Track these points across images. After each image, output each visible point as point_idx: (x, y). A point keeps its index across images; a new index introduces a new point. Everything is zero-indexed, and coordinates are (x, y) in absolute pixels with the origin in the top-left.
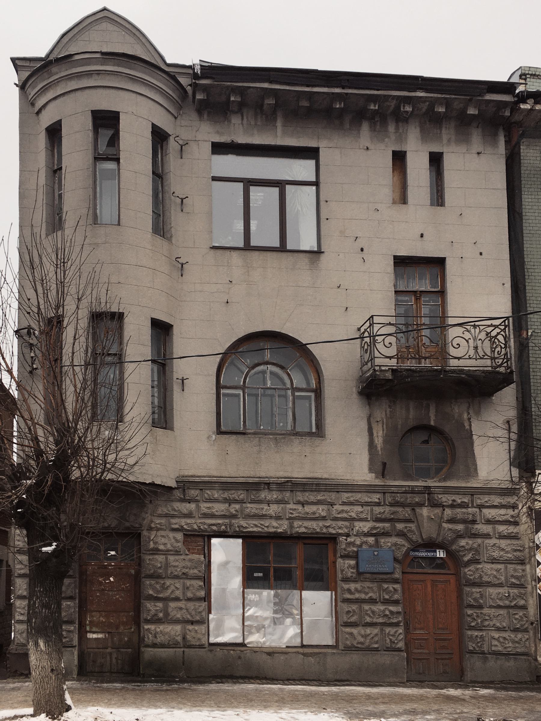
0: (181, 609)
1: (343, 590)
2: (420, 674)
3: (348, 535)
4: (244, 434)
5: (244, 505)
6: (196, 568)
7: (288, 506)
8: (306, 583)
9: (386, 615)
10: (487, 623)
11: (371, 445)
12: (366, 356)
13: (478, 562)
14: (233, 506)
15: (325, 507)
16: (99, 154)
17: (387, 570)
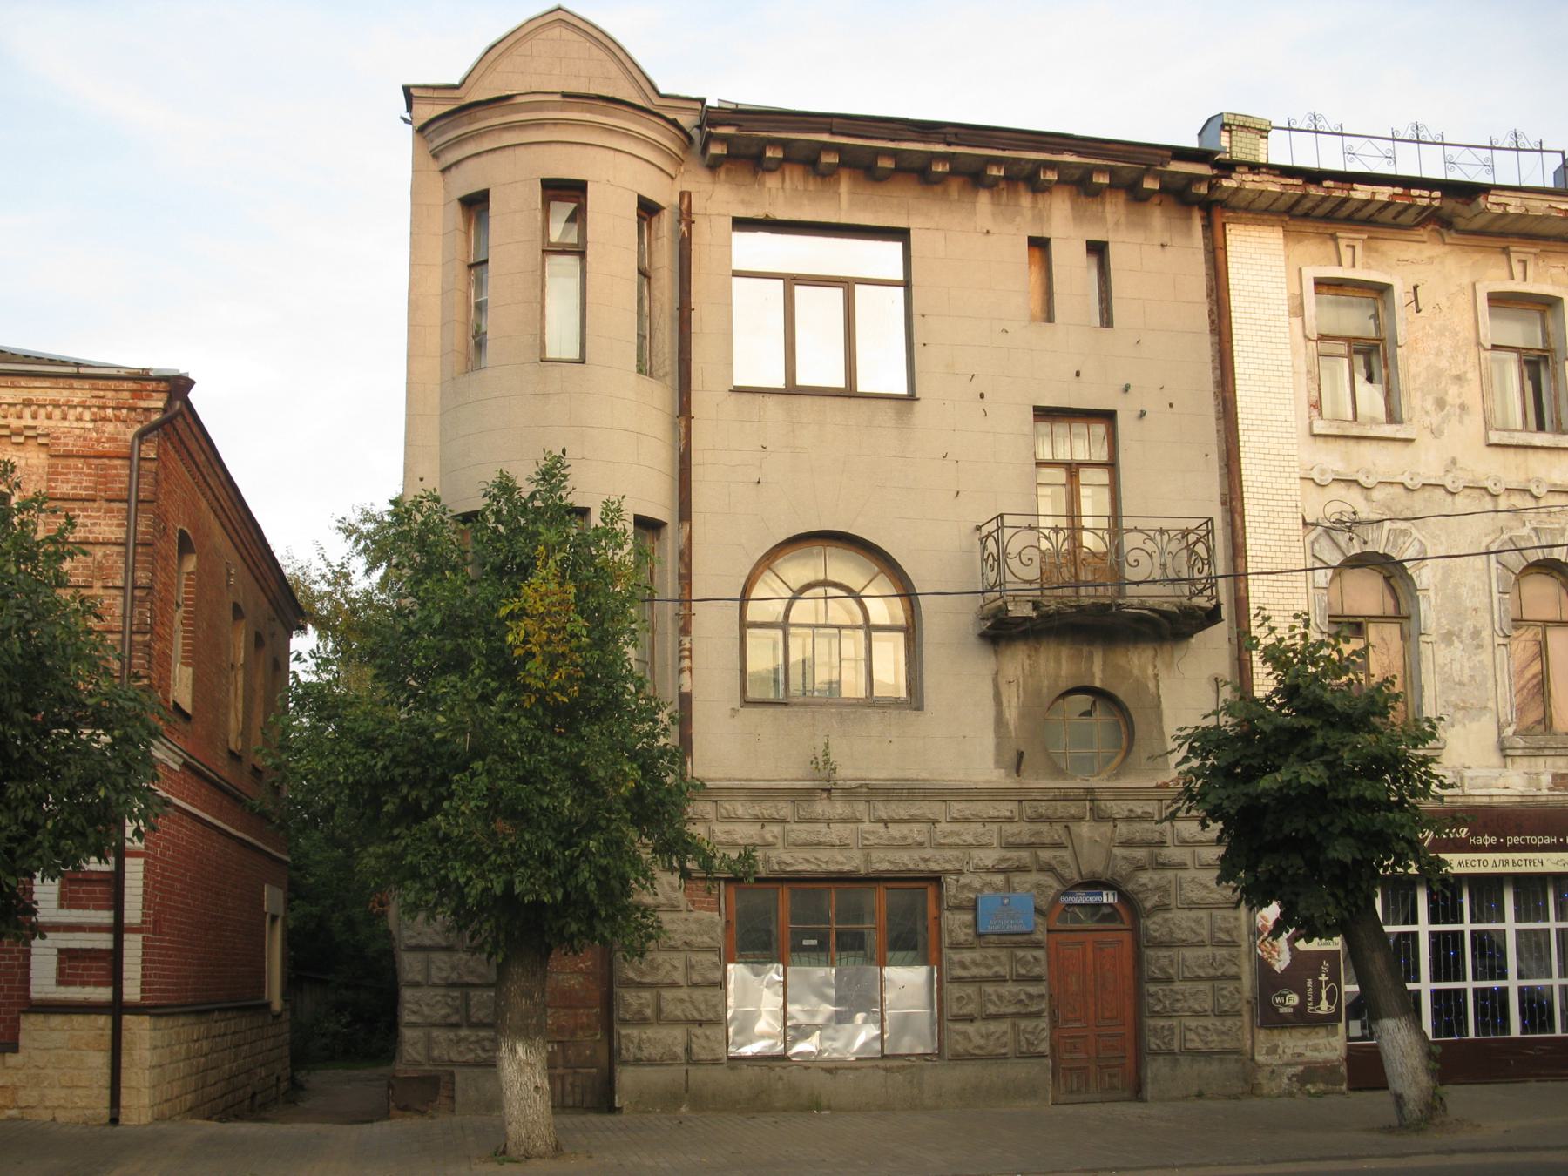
0: (682, 1001)
1: (951, 963)
2: (1072, 1092)
3: (960, 872)
4: (786, 704)
5: (788, 826)
6: (707, 933)
7: (861, 826)
8: (889, 955)
9: (1021, 1001)
10: (1179, 1005)
11: (1000, 722)
12: (992, 577)
13: (1165, 908)
14: (768, 827)
15: (925, 827)
16: (550, 244)
17: (1024, 928)
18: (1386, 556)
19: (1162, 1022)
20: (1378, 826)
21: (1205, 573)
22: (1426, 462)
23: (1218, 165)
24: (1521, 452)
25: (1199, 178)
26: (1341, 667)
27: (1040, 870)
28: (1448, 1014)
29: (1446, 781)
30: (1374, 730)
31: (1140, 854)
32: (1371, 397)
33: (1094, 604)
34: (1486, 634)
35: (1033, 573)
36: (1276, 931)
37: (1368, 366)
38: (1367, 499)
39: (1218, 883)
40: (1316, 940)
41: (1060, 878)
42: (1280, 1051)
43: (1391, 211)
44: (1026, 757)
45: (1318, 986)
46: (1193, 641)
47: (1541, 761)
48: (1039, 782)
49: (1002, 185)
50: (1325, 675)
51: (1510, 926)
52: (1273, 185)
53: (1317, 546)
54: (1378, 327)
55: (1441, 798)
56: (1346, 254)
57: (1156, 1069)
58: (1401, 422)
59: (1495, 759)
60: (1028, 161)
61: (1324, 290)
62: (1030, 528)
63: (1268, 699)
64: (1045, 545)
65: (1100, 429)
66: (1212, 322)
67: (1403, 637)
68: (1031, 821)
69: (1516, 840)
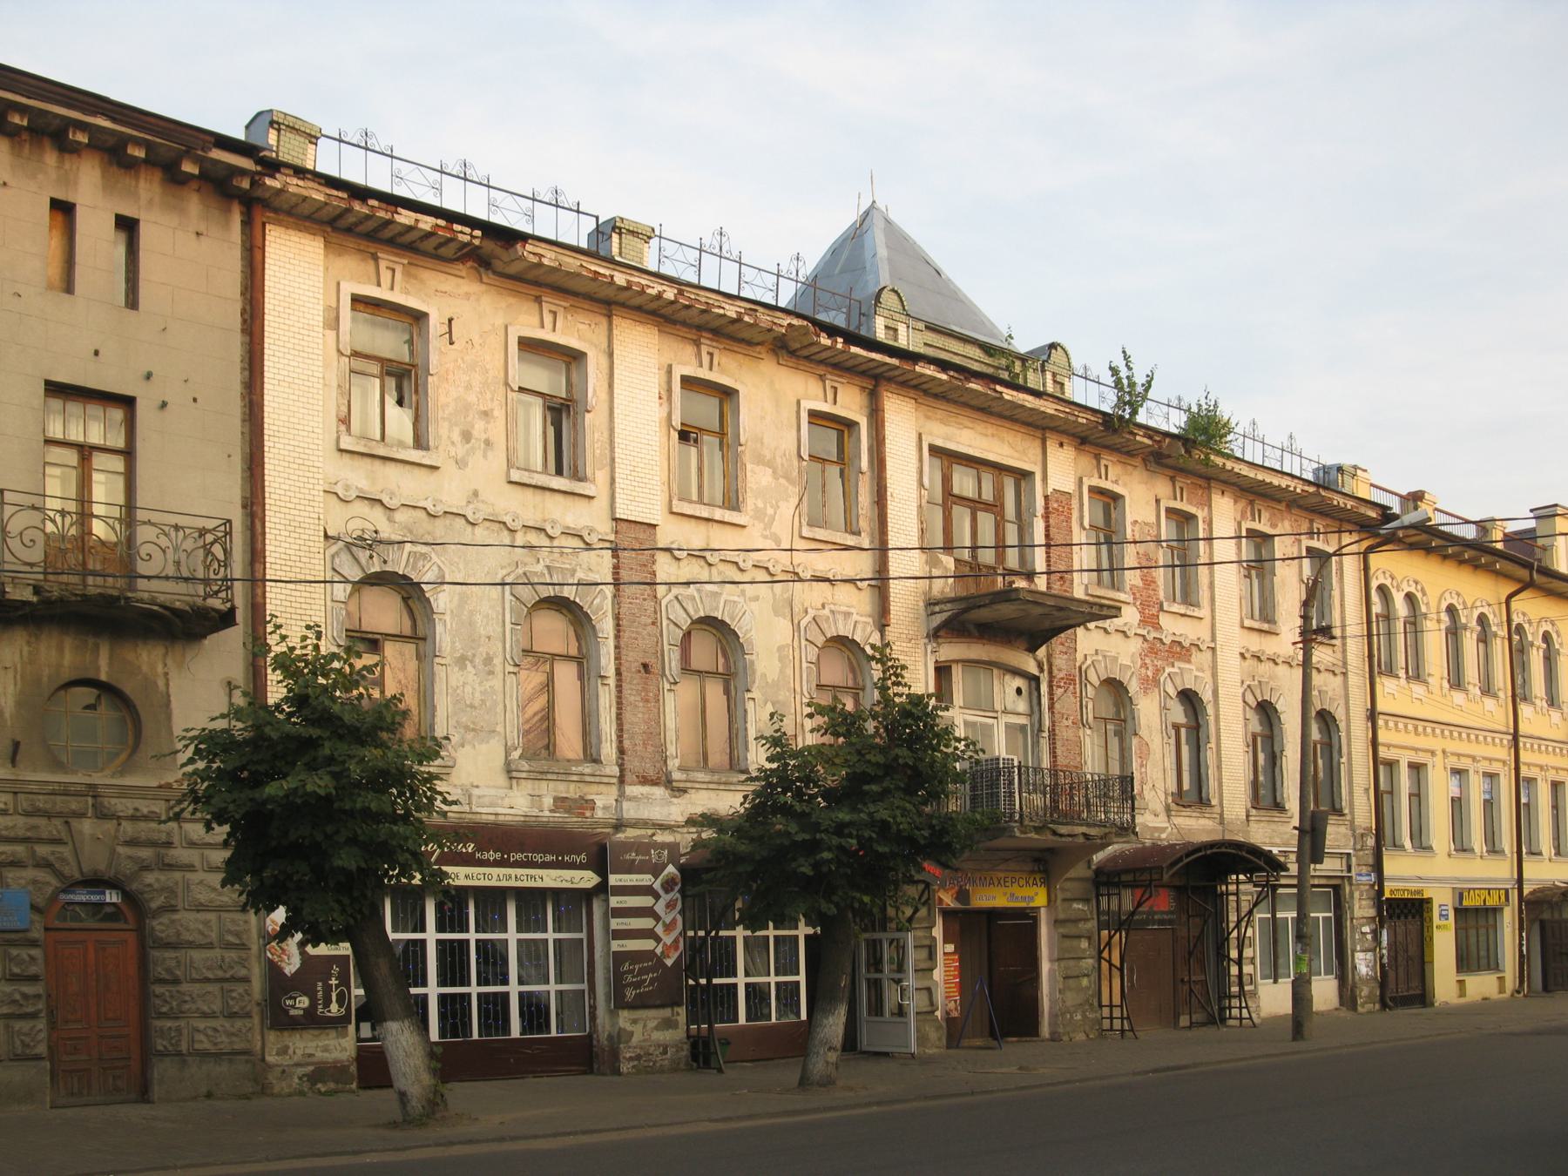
9: (14, 1002)
13: (171, 909)
17: (20, 926)
18: (404, 577)
19: (169, 1024)
20: (383, 837)
21: (221, 575)
22: (449, 490)
23: (261, 161)
24: (539, 492)
25: (243, 172)
26: (350, 681)
27: (37, 866)
28: (454, 1017)
29: (450, 798)
30: (382, 745)
31: (146, 853)
32: (400, 421)
33: (100, 594)
34: (498, 661)
35: (36, 555)
36: (285, 932)
37: (399, 389)
38: (390, 520)
39: (223, 886)
40: (323, 945)
41: (58, 874)
42: (290, 1051)
43: (433, 242)
44: (22, 748)
45: (328, 990)
46: (206, 642)
47: (544, 784)
48: (36, 775)
49: (25, 136)
50: (335, 686)
51: (512, 936)
52: (318, 194)
53: (337, 560)
54: (411, 353)
55: (444, 814)
56: (386, 276)
57: (162, 1070)
58: (427, 448)
59: (502, 780)
60: (57, 116)
61: (361, 307)
62: (34, 508)
63: (278, 706)
64: (50, 527)
65: (117, 414)
66: (244, 321)
67: (418, 657)
68: (27, 814)
69: (519, 856)
